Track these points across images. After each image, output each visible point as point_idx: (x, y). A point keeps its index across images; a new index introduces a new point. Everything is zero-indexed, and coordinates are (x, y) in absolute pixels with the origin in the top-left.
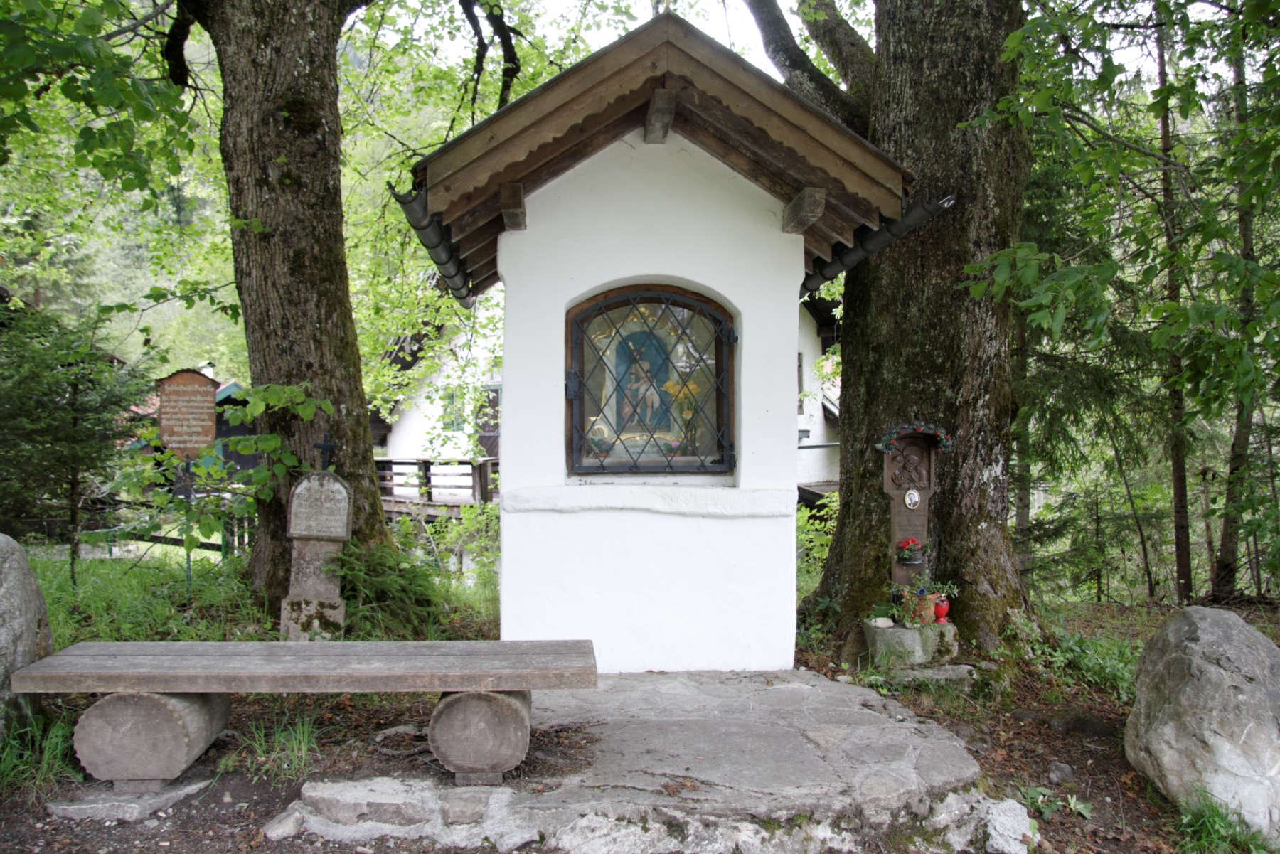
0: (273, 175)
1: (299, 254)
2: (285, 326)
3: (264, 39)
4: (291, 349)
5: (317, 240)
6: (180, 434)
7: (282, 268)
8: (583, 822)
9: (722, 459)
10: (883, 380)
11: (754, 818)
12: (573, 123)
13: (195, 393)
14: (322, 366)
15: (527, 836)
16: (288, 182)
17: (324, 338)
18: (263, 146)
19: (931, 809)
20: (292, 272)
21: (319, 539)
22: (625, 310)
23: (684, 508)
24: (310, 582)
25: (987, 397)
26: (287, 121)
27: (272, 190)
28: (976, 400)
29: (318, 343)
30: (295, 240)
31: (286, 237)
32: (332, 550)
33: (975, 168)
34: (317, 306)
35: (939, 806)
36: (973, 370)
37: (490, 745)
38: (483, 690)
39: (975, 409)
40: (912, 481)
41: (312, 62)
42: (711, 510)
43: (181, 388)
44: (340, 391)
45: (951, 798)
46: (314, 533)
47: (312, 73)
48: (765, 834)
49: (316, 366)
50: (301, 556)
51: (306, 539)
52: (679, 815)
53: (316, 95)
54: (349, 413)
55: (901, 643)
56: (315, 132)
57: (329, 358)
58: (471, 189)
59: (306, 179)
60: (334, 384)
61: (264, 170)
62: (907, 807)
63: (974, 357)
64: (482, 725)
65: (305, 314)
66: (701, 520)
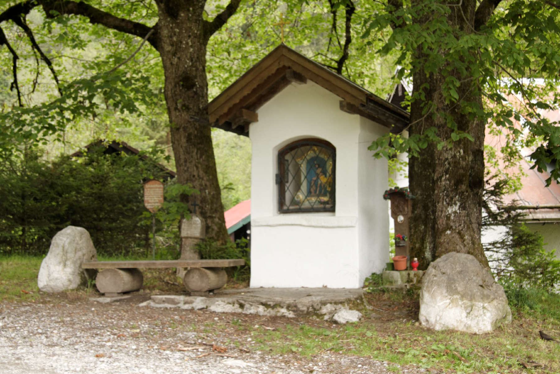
0: (179, 106)
1: (189, 135)
2: (186, 161)
3: (174, 54)
4: (188, 170)
5: (196, 129)
6: (151, 203)
7: (184, 140)
8: (217, 303)
9: (330, 207)
10: (415, 171)
11: (263, 304)
12: (253, 88)
13: (156, 188)
14: (199, 176)
15: (202, 306)
16: (184, 108)
17: (199, 166)
18: (176, 95)
19: (321, 308)
20: (187, 141)
21: (191, 238)
22: (308, 147)
23: (313, 224)
24: (188, 253)
25: (448, 176)
26: (183, 85)
27: (179, 111)
28: (441, 177)
29: (197, 167)
30: (188, 129)
31: (185, 129)
32: (196, 241)
33: (435, 77)
34: (197, 153)
35: (323, 307)
36: (439, 164)
37: (199, 283)
38: (197, 267)
39: (441, 181)
40: (401, 212)
41: (192, 61)
42: (323, 224)
43: (152, 186)
44: (206, 185)
45: (329, 305)
46: (189, 236)
47: (192, 66)
48: (266, 309)
49: (196, 177)
50: (185, 244)
51: (187, 238)
52: (243, 302)
53: (194, 74)
54: (209, 193)
55: (392, 277)
56: (193, 88)
57: (201, 173)
58: (222, 114)
59: (191, 106)
60: (203, 183)
61: (176, 104)
62: (312, 306)
63: (439, 159)
64: (197, 277)
65: (192, 157)
66: (323, 229)
